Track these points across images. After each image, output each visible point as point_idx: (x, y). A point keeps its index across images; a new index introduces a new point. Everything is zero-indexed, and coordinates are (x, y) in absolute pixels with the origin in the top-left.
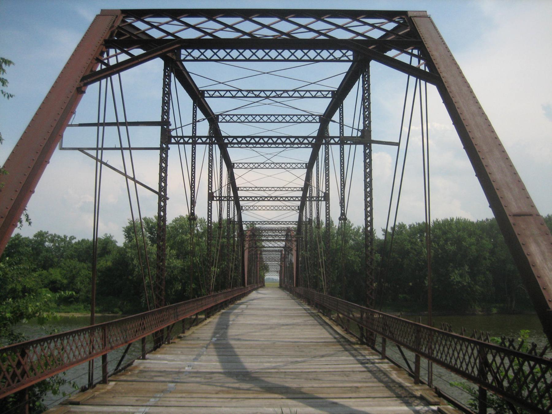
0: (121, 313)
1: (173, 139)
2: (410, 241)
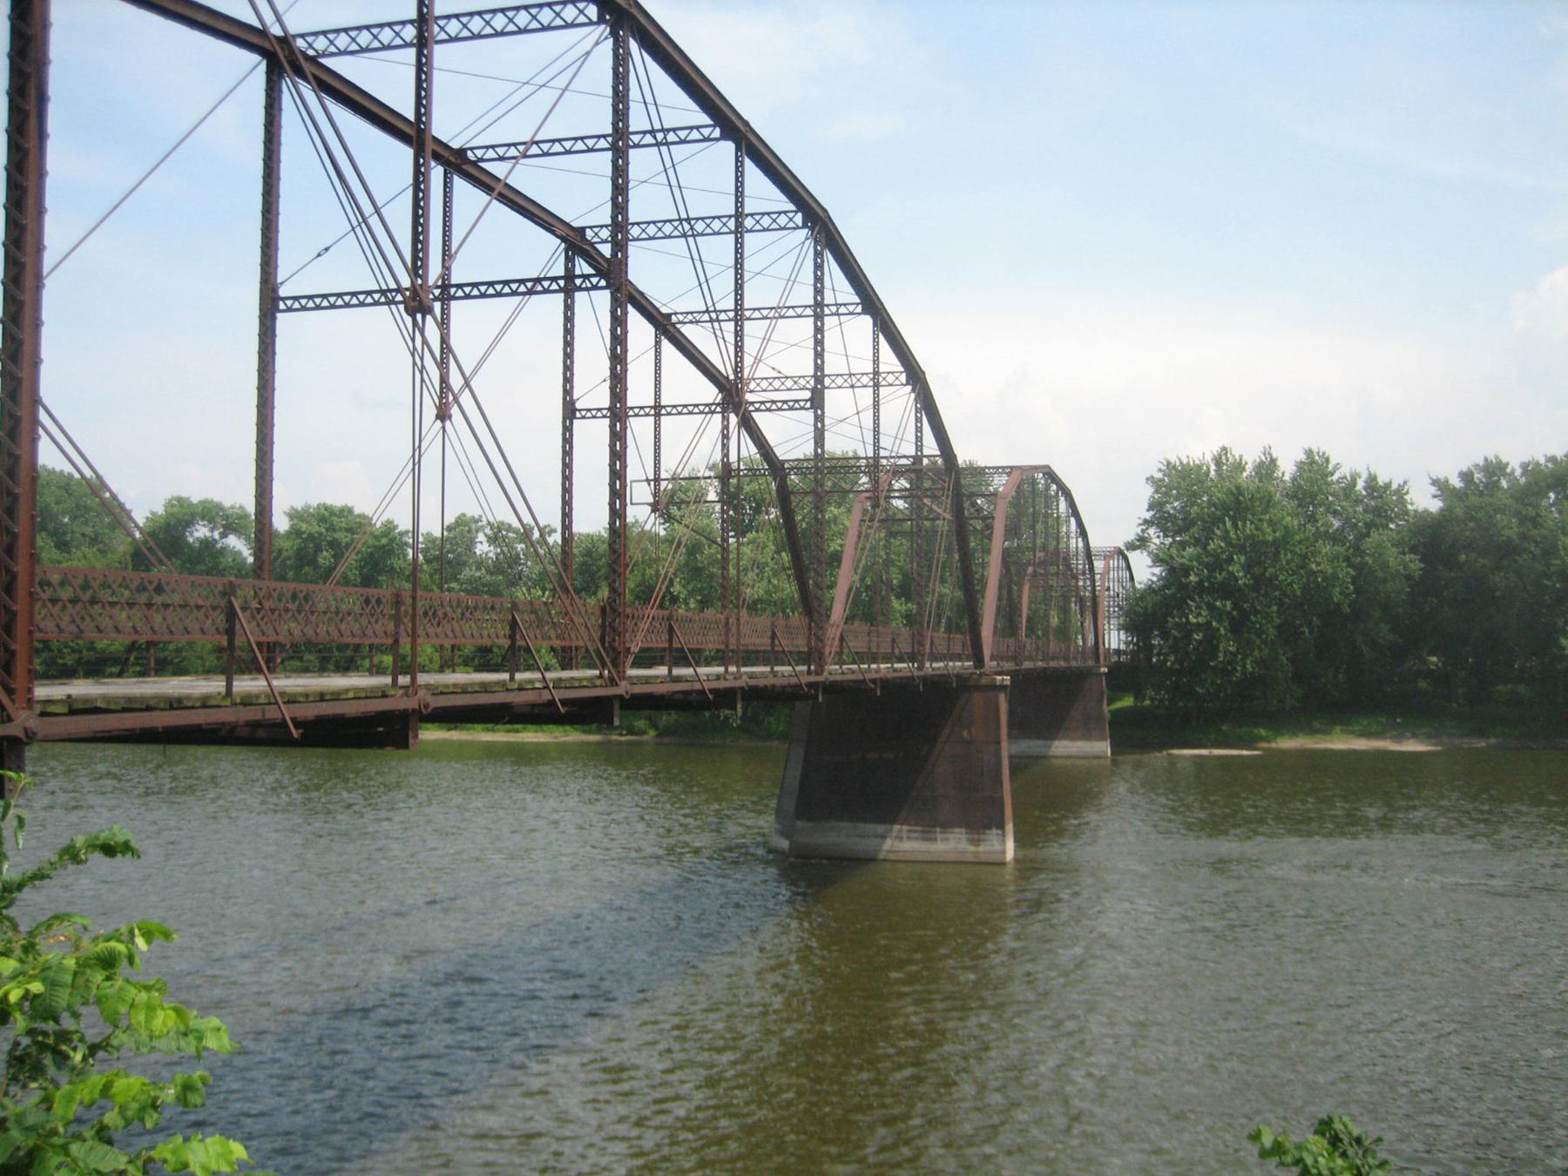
0: (652, 733)
1: (281, 303)
2: (1517, 514)
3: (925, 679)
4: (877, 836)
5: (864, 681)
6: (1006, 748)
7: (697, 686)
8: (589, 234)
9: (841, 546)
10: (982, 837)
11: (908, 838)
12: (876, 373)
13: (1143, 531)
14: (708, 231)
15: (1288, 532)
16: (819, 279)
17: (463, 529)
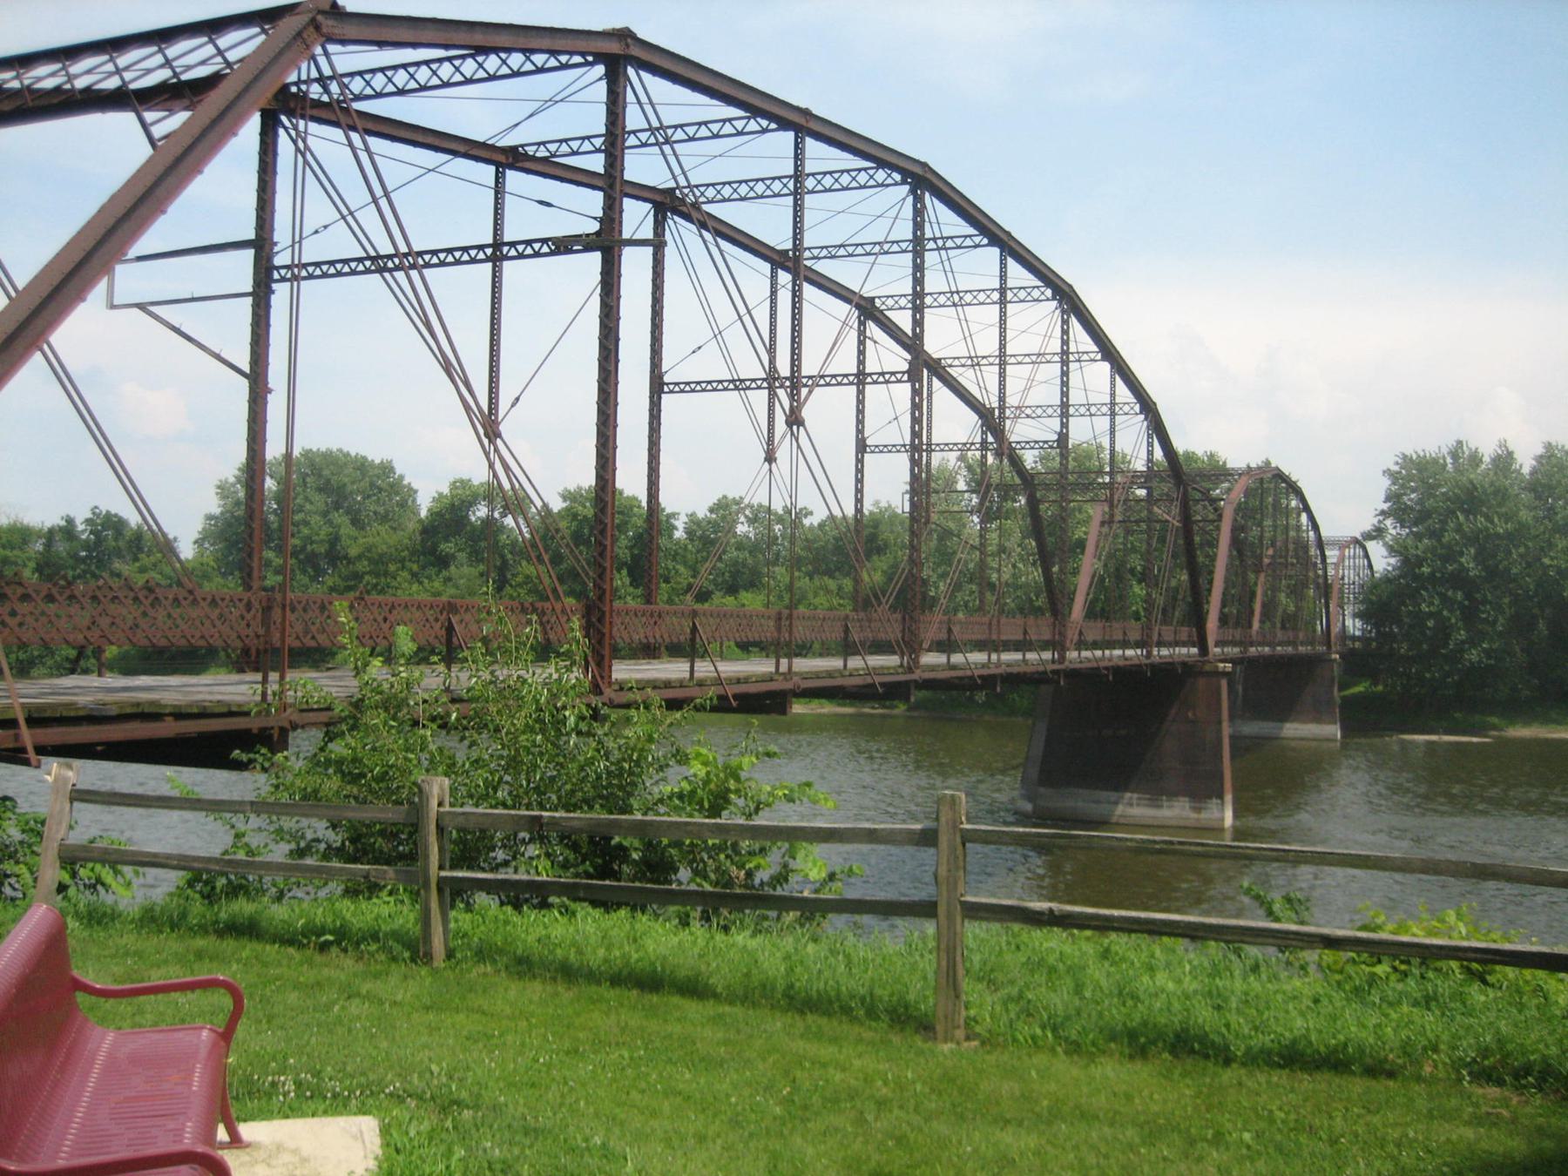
3: (1153, 666)
4: (1109, 802)
5: (1098, 669)
6: (1226, 730)
7: (969, 673)
8: (878, 303)
9: (1086, 533)
10: (1203, 805)
11: (1138, 805)
12: (1113, 404)
13: (1380, 522)
14: (975, 301)
15: (1522, 527)
16: (1065, 332)
17: (725, 509)
